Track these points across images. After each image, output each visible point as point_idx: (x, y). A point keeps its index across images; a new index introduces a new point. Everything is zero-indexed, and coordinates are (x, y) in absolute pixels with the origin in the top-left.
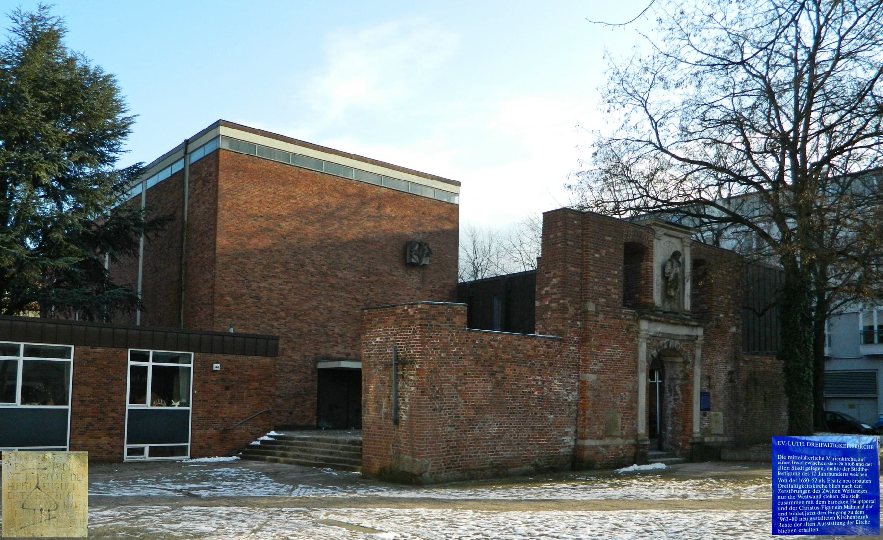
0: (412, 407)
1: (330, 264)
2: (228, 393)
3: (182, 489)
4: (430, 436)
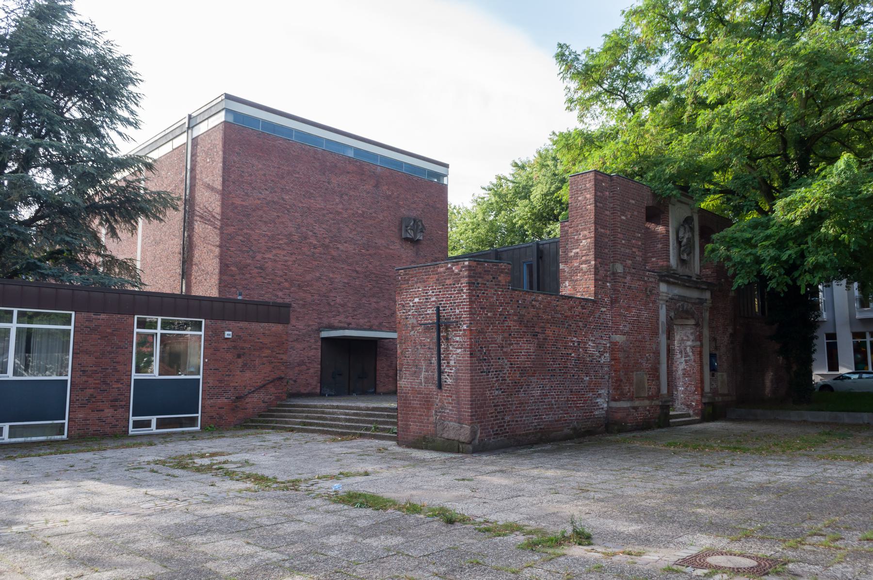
0: (458, 370)
1: (332, 237)
2: (240, 361)
3: (212, 465)
4: (479, 400)
